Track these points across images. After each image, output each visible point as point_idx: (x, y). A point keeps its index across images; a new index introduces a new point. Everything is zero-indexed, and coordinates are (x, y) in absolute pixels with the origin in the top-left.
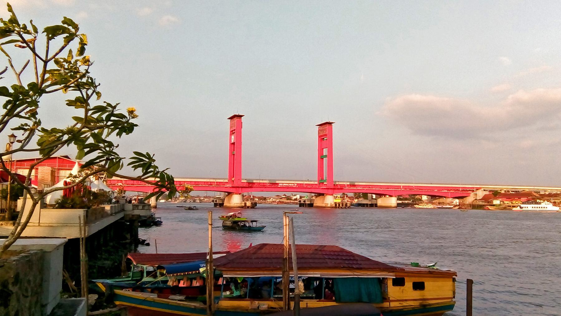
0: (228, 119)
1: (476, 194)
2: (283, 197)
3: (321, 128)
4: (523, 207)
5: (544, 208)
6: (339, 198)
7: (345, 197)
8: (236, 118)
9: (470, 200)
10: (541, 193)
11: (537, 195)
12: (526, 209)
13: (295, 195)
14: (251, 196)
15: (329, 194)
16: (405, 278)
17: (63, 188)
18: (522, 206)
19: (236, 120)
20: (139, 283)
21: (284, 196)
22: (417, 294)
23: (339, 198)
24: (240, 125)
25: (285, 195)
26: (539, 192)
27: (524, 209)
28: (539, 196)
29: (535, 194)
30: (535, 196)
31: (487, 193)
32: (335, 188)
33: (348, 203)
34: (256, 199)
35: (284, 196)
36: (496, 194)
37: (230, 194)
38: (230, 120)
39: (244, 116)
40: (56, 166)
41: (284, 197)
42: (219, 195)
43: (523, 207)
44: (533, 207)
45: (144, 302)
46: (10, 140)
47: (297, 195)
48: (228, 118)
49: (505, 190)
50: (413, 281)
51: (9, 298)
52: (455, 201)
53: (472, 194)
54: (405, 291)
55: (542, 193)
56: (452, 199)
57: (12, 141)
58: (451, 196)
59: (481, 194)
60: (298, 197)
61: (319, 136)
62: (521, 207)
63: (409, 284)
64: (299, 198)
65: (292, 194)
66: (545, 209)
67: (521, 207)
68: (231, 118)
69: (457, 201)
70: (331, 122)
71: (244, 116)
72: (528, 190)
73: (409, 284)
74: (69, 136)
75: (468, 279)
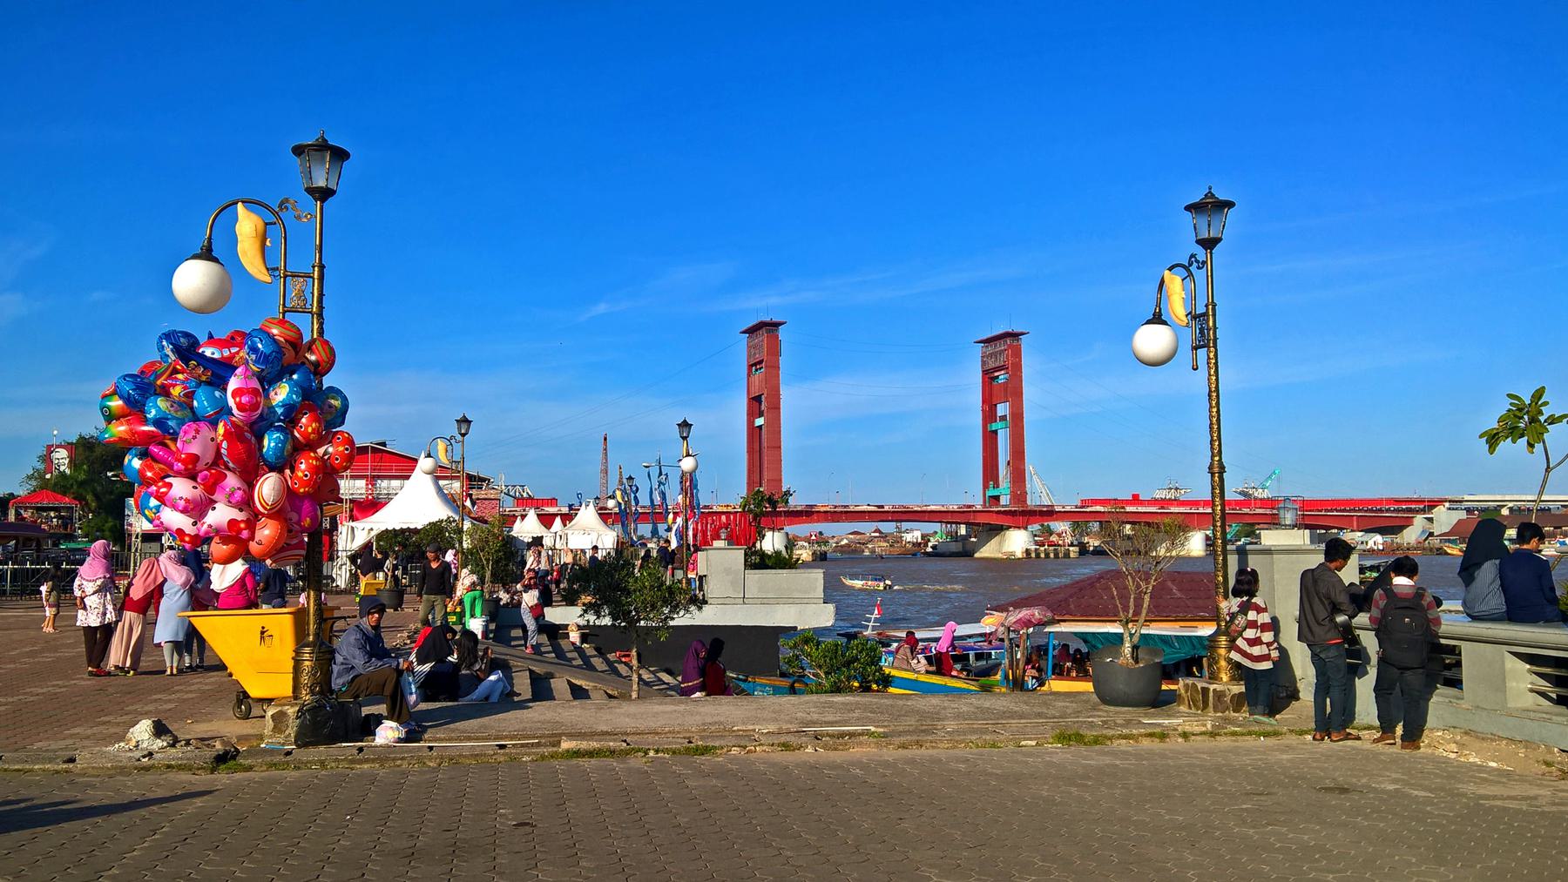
1: (1432, 518)
3: (990, 350)
15: (1015, 527)
17: (1056, 520)
20: (690, 684)
21: (877, 534)
24: (775, 350)
25: (880, 532)
32: (1023, 515)
33: (1071, 549)
35: (877, 534)
38: (748, 335)
39: (785, 323)
40: (368, 469)
46: (459, 429)
47: (915, 532)
48: (745, 328)
49: (1511, 505)
53: (1419, 520)
57: (463, 431)
60: (917, 534)
68: (751, 331)
70: (1017, 330)
74: (296, 383)
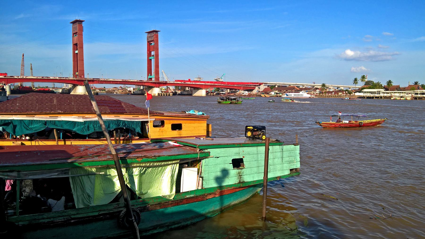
0: (70, 23)
2: (120, 89)
4: (288, 95)
5: (301, 95)
6: (164, 90)
7: (169, 89)
8: (77, 23)
9: (255, 92)
10: (300, 87)
11: (298, 89)
12: (290, 96)
13: (129, 87)
14: (93, 88)
16: (164, 120)
18: (288, 94)
19: (77, 25)
21: (121, 88)
22: (175, 133)
23: (164, 90)
24: (81, 29)
25: (122, 88)
26: (299, 87)
27: (289, 96)
28: (299, 89)
29: (297, 88)
30: (297, 89)
31: (266, 87)
34: (97, 90)
35: (121, 88)
36: (272, 87)
37: (75, 86)
41: (121, 89)
42: (65, 86)
43: (288, 95)
44: (294, 95)
45: (304, 231)
49: (278, 85)
50: (172, 123)
51: (48, 204)
52: (246, 93)
53: (257, 88)
54: (164, 131)
55: (301, 87)
56: (243, 91)
58: (243, 89)
59: (262, 88)
61: (147, 41)
62: (287, 95)
63: (168, 126)
64: (132, 90)
65: (127, 86)
66: (302, 96)
67: (287, 95)
69: (246, 93)
70: (157, 30)
71: (84, 21)
72: (292, 85)
73: (168, 126)
75: (151, 60)
